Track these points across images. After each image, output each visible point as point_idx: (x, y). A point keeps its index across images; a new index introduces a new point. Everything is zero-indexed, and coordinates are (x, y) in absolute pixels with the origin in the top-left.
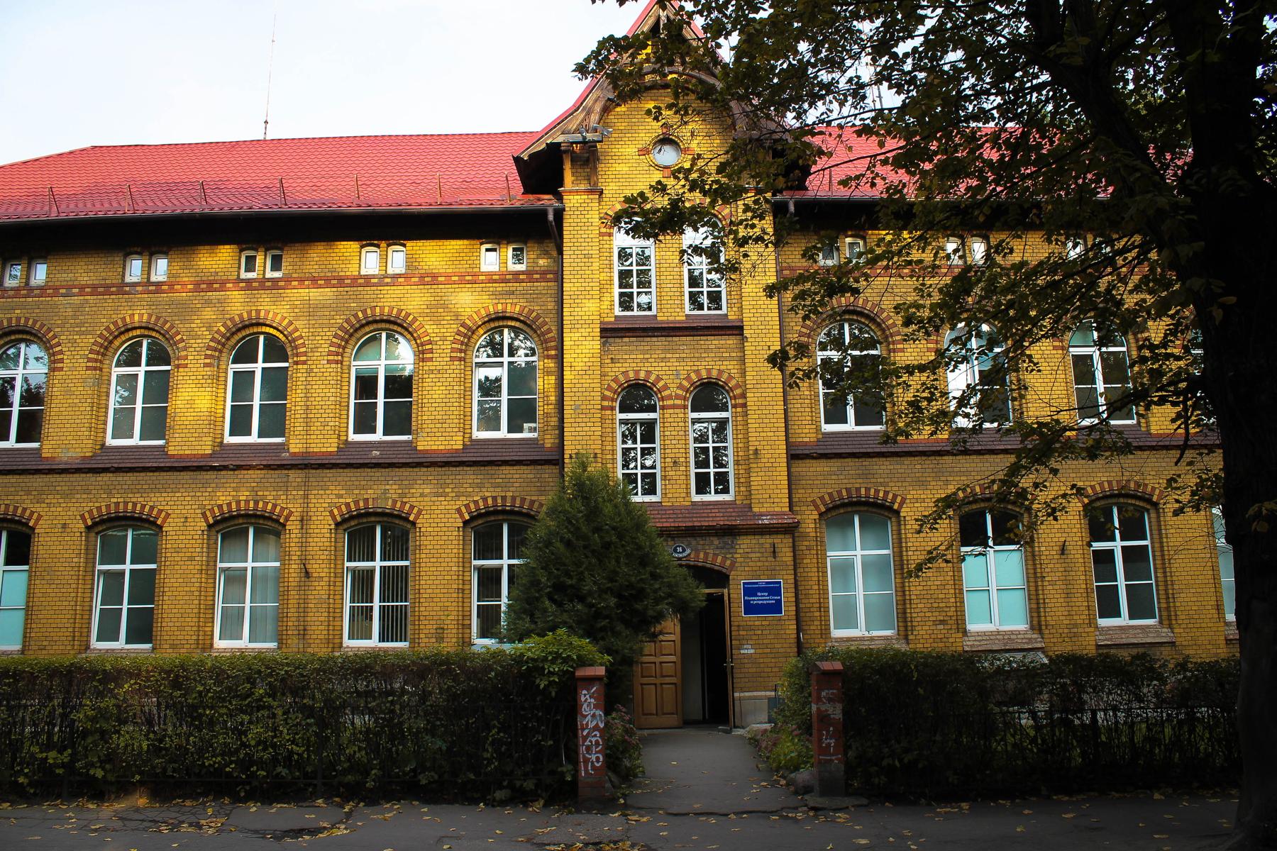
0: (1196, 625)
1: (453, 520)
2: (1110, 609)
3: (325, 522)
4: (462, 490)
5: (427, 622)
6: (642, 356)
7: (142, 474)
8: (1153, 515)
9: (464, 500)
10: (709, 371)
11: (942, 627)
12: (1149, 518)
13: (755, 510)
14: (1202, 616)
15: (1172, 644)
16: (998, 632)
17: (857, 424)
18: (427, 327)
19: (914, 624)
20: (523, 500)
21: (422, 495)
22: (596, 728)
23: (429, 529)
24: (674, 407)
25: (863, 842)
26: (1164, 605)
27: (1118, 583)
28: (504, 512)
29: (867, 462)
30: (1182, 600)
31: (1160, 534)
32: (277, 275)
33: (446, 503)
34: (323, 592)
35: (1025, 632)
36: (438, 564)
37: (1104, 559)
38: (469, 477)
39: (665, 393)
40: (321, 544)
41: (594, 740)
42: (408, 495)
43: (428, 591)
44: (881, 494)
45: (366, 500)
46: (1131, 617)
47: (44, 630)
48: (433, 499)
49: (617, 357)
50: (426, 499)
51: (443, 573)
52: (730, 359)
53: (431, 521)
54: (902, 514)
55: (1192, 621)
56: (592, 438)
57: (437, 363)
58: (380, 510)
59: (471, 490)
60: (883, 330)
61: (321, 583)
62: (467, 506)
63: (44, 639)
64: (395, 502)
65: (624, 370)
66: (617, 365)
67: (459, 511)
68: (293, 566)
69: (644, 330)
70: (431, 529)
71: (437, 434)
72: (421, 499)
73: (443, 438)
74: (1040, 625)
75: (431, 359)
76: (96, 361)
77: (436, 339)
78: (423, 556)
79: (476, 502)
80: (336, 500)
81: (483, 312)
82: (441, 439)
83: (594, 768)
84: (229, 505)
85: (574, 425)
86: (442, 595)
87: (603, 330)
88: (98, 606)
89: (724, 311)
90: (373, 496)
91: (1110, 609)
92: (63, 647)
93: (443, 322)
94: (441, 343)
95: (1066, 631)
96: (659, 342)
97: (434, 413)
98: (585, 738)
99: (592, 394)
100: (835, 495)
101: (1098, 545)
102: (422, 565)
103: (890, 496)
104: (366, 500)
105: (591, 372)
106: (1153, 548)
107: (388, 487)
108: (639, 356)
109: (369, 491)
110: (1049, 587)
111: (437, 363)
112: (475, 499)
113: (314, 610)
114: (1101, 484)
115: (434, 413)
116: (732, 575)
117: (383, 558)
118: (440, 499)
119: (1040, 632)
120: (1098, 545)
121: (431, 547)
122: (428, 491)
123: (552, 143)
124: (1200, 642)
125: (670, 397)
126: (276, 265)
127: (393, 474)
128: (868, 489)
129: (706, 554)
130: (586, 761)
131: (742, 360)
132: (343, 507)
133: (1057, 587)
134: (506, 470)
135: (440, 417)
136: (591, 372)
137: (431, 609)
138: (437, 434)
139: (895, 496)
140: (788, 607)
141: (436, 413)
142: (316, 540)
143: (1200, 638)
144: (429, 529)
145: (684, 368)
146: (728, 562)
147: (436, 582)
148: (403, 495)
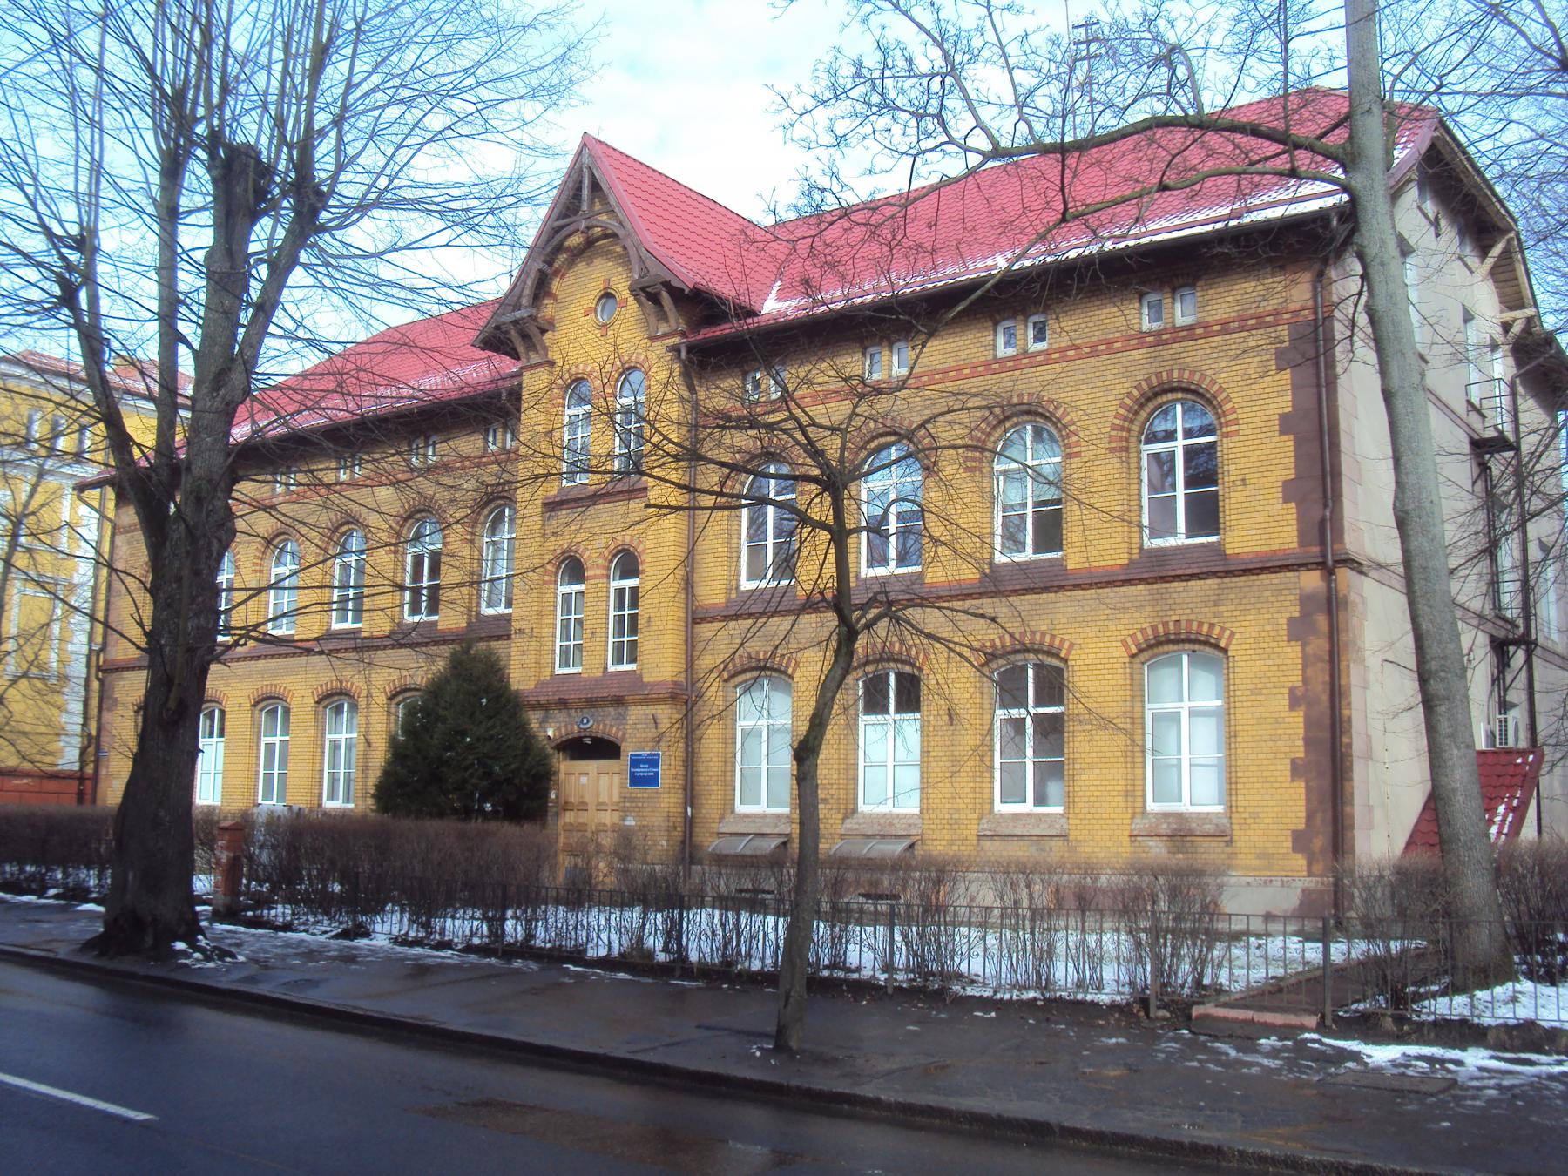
0: (1096, 816)
7: (1243, 578)
14: (1104, 805)
15: (1064, 837)
18: (1220, 381)
25: (1446, 1124)
27: (1027, 760)
30: (1082, 783)
32: (1041, 346)
54: (1230, 653)
55: (1092, 810)
76: (974, 459)
87: (545, 504)
88: (262, 771)
95: (947, 816)
101: (287, 738)
110: (933, 764)
116: (623, 746)
120: (287, 738)
124: (1098, 838)
126: (1040, 336)
129: (605, 725)
133: (942, 764)
143: (1100, 833)
146: (620, 733)
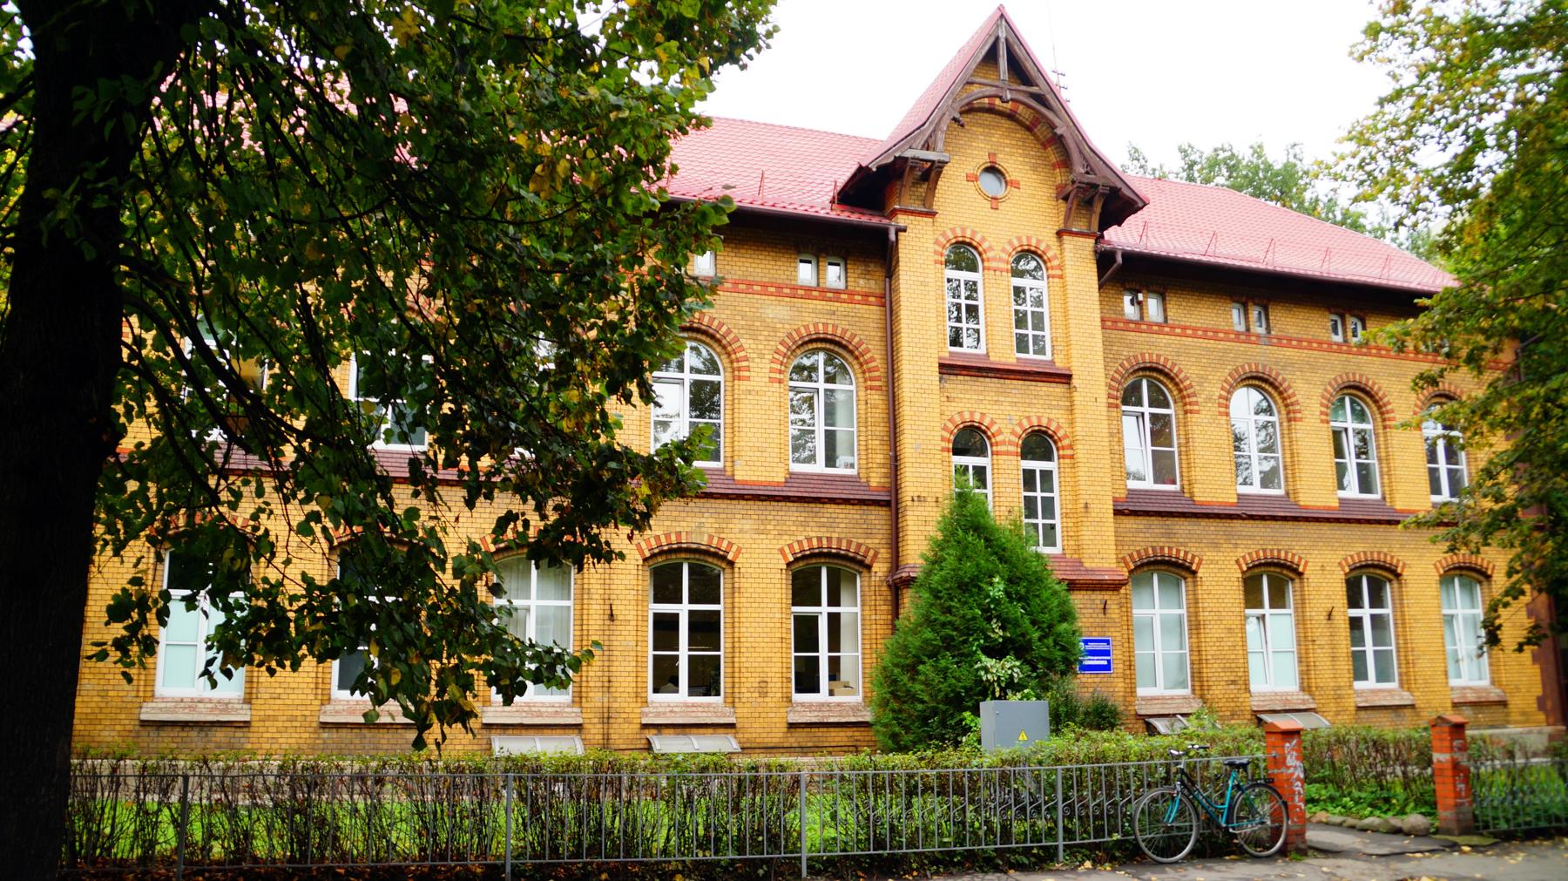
2: (1360, 674)
8: (1297, 585)
9: (786, 540)
10: (1039, 418)
13: (1087, 565)
15: (1412, 706)
17: (1156, 481)
20: (849, 543)
24: (1007, 453)
28: (821, 555)
29: (1170, 521)
31: (1402, 604)
34: (630, 638)
37: (1356, 623)
38: (793, 513)
39: (999, 438)
40: (627, 582)
44: (1182, 554)
45: (679, 534)
52: (1058, 407)
58: (694, 546)
59: (794, 528)
60: (1180, 391)
61: (628, 628)
62: (790, 546)
64: (711, 537)
67: (782, 551)
68: (594, 607)
69: (979, 369)
72: (739, 536)
74: (1309, 687)
75: (748, 378)
78: (742, 600)
79: (800, 542)
81: (1339, 381)
87: (942, 366)
89: (1048, 357)
91: (1360, 674)
92: (304, 697)
96: (991, 384)
100: (1143, 552)
102: (743, 610)
103: (1189, 557)
104: (679, 534)
106: (1395, 616)
107: (703, 520)
109: (682, 524)
112: (800, 538)
113: (620, 658)
114: (1358, 554)
119: (1310, 693)
123: (900, 157)
125: (1003, 443)
127: (708, 505)
128: (1170, 549)
131: (1071, 409)
134: (831, 508)
139: (1193, 557)
140: (1118, 667)
142: (621, 577)
148: (720, 530)
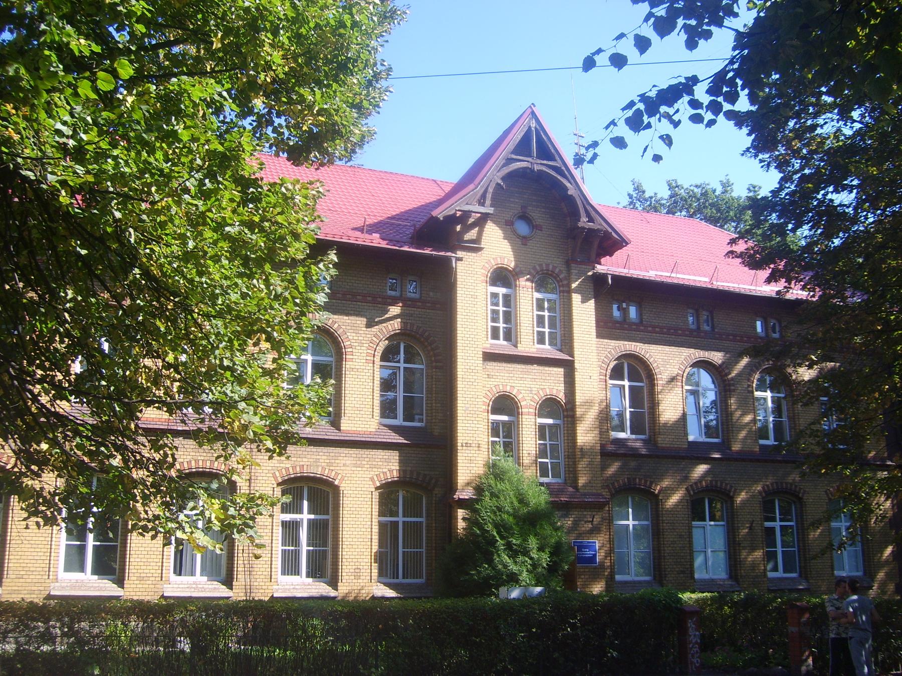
1: (368, 486)
3: (269, 482)
4: (374, 463)
5: (348, 564)
6: (508, 375)
9: (376, 471)
11: (682, 575)
12: (795, 508)
16: (713, 580)
19: (667, 573)
21: (344, 465)
22: (696, 643)
23: (350, 492)
26: (803, 565)
33: (363, 472)
35: (724, 580)
36: (357, 519)
41: (695, 650)
42: (334, 465)
43: (349, 540)
46: (785, 571)
47: (21, 561)
48: (353, 469)
49: (492, 374)
50: (348, 468)
51: (360, 526)
53: (351, 485)
54: (660, 498)
56: (477, 432)
57: (357, 364)
63: (21, 569)
64: (324, 469)
65: (496, 383)
66: (492, 380)
67: (372, 479)
70: (351, 492)
71: (356, 419)
73: (360, 422)
77: (355, 344)
79: (197, 461)
80: (278, 465)
82: (359, 422)
83: (696, 667)
84: (189, 463)
85: (464, 422)
86: (359, 543)
90: (307, 463)
93: (360, 332)
94: (359, 348)
97: (353, 402)
98: (691, 649)
99: (477, 400)
105: (476, 384)
108: (506, 375)
111: (357, 364)
112: (384, 470)
115: (353, 402)
117: (404, 516)
118: (358, 469)
121: (351, 506)
122: (349, 462)
130: (692, 663)
132: (284, 471)
135: (358, 406)
136: (476, 384)
137: (350, 553)
138: (356, 419)
141: (355, 402)
144: (350, 492)
145: (535, 387)
147: (354, 533)
